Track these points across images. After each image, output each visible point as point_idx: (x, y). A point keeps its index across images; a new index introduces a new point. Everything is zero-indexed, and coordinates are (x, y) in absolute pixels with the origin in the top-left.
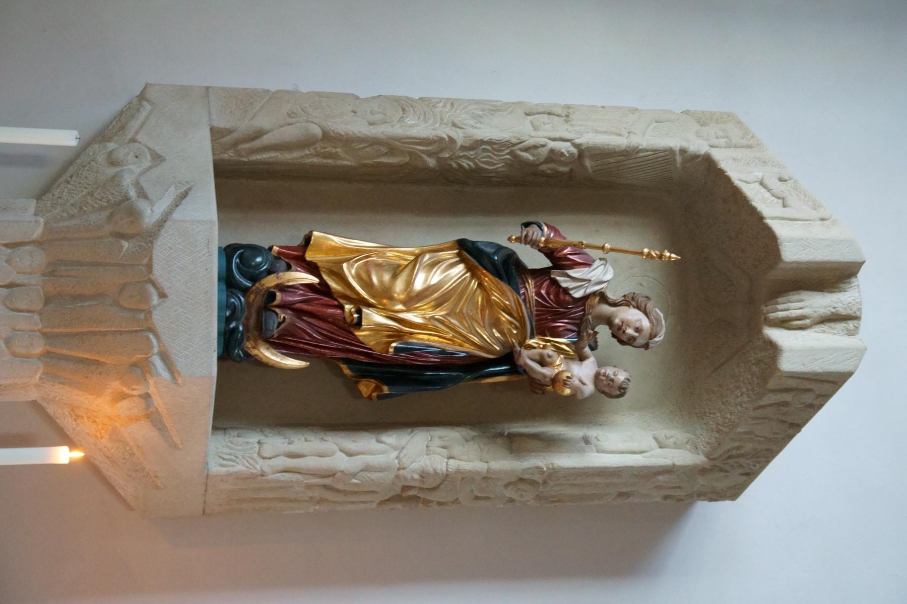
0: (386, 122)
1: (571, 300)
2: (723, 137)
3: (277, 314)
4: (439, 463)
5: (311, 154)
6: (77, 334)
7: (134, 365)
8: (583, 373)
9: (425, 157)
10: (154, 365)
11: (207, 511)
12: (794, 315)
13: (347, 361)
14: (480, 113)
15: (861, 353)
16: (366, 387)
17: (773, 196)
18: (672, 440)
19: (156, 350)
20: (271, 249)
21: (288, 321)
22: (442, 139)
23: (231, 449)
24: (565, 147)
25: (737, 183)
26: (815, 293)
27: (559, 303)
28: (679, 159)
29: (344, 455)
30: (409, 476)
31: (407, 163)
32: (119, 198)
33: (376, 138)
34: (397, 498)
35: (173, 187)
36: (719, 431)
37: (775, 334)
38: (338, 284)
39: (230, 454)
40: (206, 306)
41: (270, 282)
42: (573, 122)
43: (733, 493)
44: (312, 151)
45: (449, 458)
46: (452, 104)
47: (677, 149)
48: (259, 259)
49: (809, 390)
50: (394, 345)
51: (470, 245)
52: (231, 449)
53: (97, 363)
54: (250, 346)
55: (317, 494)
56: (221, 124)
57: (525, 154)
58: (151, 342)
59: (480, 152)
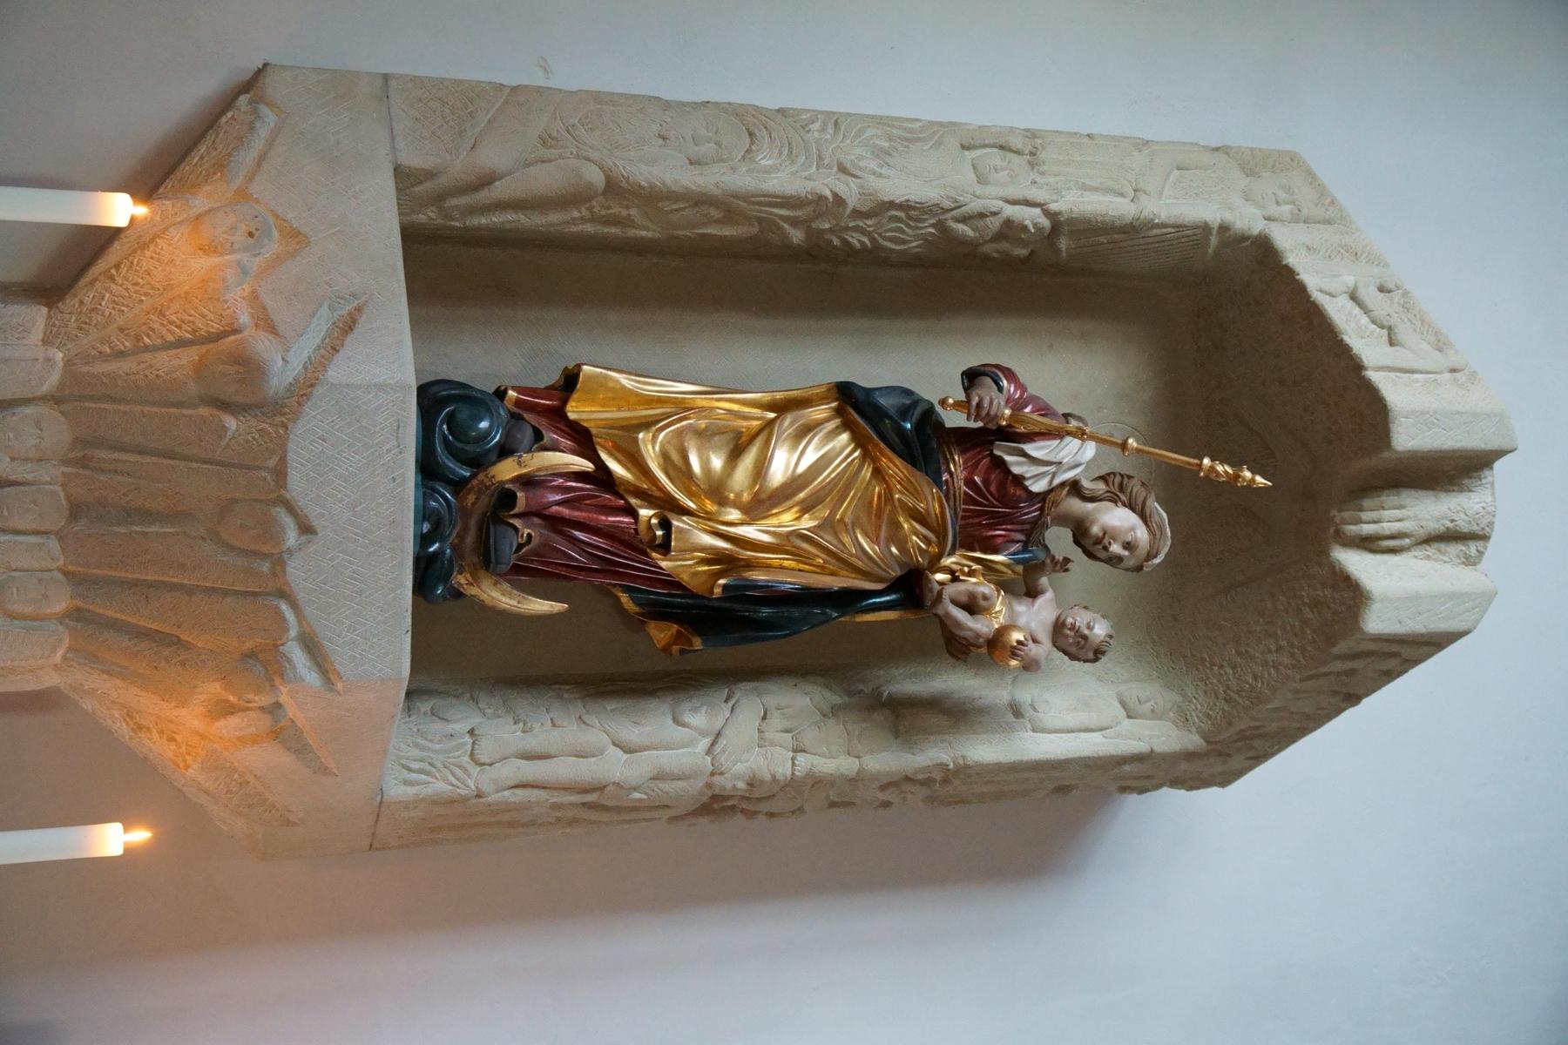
1: (1024, 495)
4: (777, 762)
5: (582, 218)
6: (134, 584)
7: (251, 655)
8: (1030, 619)
9: (786, 226)
10: (289, 661)
11: (376, 845)
12: (1387, 532)
13: (627, 589)
15: (1485, 600)
16: (661, 633)
17: (1374, 322)
18: (1149, 705)
19: (293, 633)
20: (500, 394)
21: (535, 541)
22: (821, 198)
23: (423, 749)
24: (1030, 217)
26: (1422, 493)
27: (1004, 499)
28: (1214, 240)
29: (619, 753)
32: (216, 327)
35: (325, 307)
37: (1355, 562)
38: (627, 469)
40: (392, 550)
42: (1043, 168)
43: (1225, 780)
44: (584, 212)
47: (1216, 226)
50: (722, 581)
51: (861, 396)
52: (423, 749)
54: (463, 581)
55: (570, 814)
56: (414, 160)
57: (961, 227)
58: (284, 619)
59: (884, 221)
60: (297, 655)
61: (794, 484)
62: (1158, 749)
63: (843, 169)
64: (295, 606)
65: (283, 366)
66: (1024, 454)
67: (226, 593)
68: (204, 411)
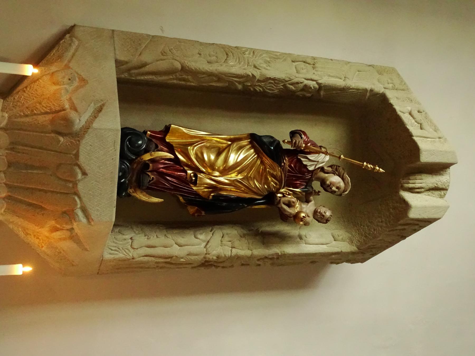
0: (217, 62)
2: (391, 83)
3: (149, 176)
6: (28, 189)
7: (65, 212)
10: (77, 215)
14: (269, 59)
15: (446, 208)
17: (416, 122)
18: (341, 237)
19: (79, 206)
20: (145, 132)
21: (155, 179)
22: (248, 75)
24: (313, 84)
25: (399, 113)
26: (428, 175)
28: (368, 94)
30: (211, 258)
31: (227, 87)
32: (58, 108)
33: (212, 73)
34: (200, 266)
36: (366, 237)
37: (407, 196)
39: (115, 247)
41: (147, 157)
42: (317, 69)
44: (174, 77)
45: (232, 248)
46: (254, 52)
47: (369, 89)
48: (140, 142)
49: (418, 225)
50: (212, 194)
52: (116, 243)
53: (42, 208)
56: (122, 58)
57: (291, 86)
58: (76, 201)
60: (80, 213)
61: (237, 164)
62: (344, 251)
63: (255, 67)
64: (79, 197)
65: (79, 122)
66: (307, 158)
67: (58, 193)
68: (53, 135)
